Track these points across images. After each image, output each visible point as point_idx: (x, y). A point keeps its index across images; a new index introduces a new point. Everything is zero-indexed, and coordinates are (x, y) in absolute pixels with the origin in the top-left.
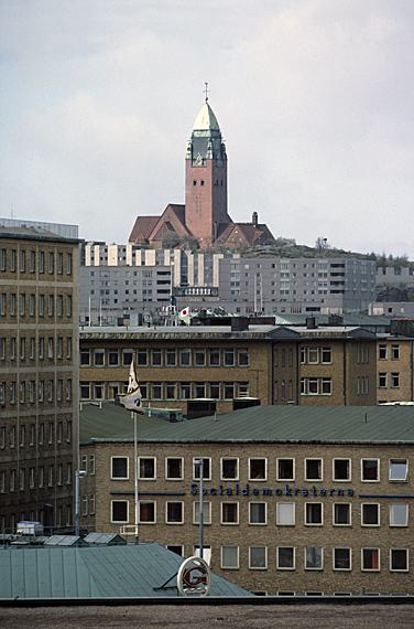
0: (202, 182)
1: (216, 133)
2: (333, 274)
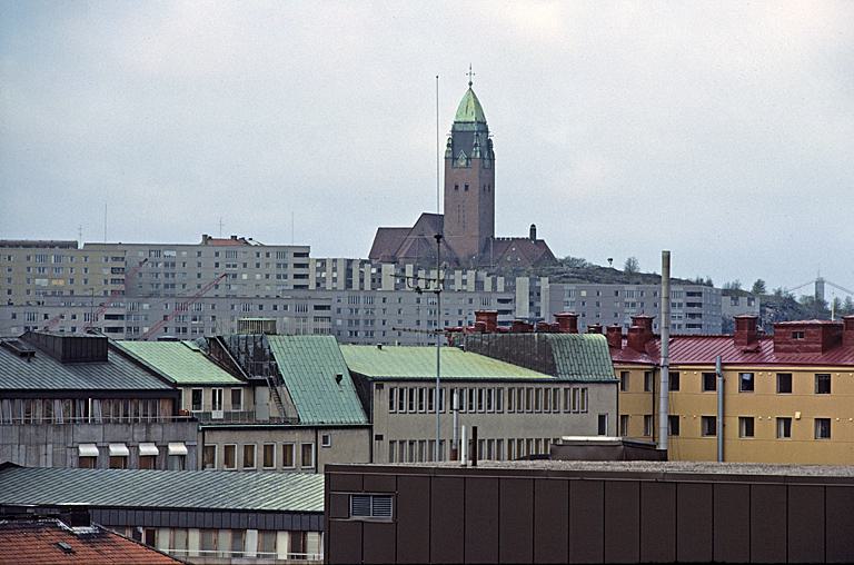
0: (467, 187)
1: (483, 127)
2: (689, 305)
